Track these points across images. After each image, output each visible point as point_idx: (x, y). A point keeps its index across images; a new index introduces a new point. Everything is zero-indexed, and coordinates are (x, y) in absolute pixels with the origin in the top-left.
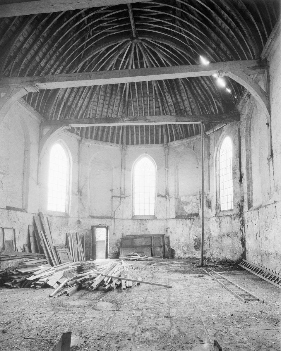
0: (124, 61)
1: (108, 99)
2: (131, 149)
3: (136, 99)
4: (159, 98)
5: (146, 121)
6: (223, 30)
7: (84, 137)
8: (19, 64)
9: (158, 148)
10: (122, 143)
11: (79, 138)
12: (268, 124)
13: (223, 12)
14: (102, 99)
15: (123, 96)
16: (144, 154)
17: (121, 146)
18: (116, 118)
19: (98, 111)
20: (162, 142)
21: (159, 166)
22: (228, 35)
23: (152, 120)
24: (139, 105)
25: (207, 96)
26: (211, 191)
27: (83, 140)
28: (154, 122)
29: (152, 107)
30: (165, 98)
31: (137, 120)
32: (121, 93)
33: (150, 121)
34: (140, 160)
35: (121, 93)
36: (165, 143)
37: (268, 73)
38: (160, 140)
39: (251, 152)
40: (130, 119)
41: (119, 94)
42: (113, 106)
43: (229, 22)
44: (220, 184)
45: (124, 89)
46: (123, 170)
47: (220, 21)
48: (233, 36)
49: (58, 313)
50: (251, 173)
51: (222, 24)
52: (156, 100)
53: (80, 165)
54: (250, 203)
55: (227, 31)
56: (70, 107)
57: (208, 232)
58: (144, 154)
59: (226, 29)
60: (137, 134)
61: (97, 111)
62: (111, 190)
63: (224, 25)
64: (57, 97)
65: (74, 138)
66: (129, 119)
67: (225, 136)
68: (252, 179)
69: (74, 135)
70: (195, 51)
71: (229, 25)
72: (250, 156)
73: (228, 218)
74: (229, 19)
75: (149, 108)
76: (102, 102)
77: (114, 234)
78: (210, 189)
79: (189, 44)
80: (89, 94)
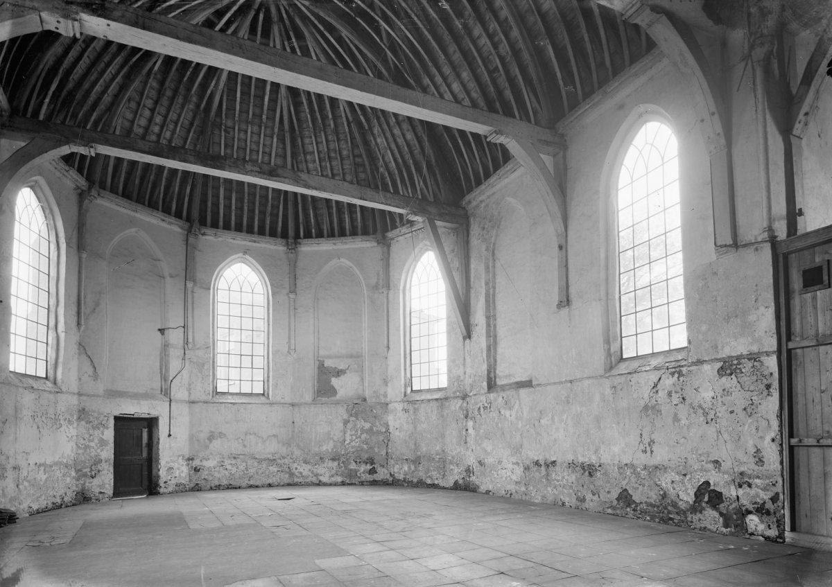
0: (212, 18)
1: (165, 102)
2: (211, 239)
3: (235, 124)
4: (288, 136)
5: (298, 182)
6: (479, 50)
7: (97, 184)
8: (601, 65)
9: (275, 247)
10: (188, 219)
11: (82, 182)
12: (561, 247)
13: (488, 16)
14: (152, 99)
15: (203, 106)
16: (240, 255)
17: (187, 225)
18: (225, 158)
19: (137, 125)
20: (284, 236)
21: (276, 288)
22: (486, 61)
23: (311, 183)
24: (239, 140)
25: (400, 161)
26: (391, 351)
27: (94, 192)
28: (316, 189)
29: (256, 149)
30: (302, 141)
31: (278, 176)
32: (201, 97)
33: (307, 186)
34: (229, 267)
35: (201, 97)
36: (290, 241)
37: (564, 157)
38: (279, 229)
39: (494, 288)
40: (261, 169)
41: (194, 99)
42: (176, 123)
43: (496, 39)
44: (413, 340)
45: (209, 92)
46: (190, 285)
47: (477, 30)
48: (497, 67)
49: (458, 554)
50: (495, 326)
51: (479, 37)
52: (282, 140)
53: (84, 256)
54: (491, 379)
55: (485, 54)
56: (71, 94)
57: (384, 430)
58: (241, 255)
59: (485, 49)
60: (251, 211)
61: (135, 125)
62: (162, 331)
63: (484, 41)
64: (45, 60)
65: (72, 180)
66: (258, 169)
67: (427, 250)
68: (495, 337)
69: (73, 173)
70: (397, 62)
71: (495, 46)
72: (494, 295)
73: (435, 404)
74: (498, 34)
75: (261, 153)
76: (149, 106)
77: (170, 435)
78: (391, 346)
79: (385, 40)
80: (121, 74)
